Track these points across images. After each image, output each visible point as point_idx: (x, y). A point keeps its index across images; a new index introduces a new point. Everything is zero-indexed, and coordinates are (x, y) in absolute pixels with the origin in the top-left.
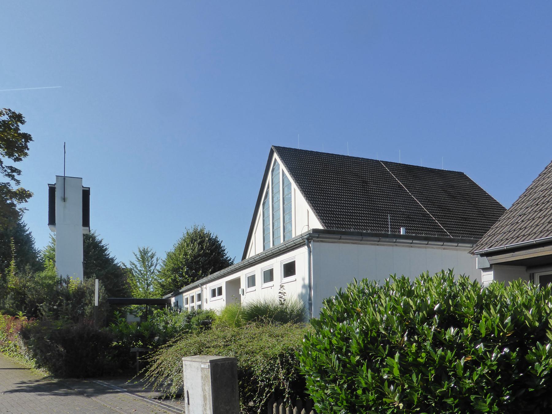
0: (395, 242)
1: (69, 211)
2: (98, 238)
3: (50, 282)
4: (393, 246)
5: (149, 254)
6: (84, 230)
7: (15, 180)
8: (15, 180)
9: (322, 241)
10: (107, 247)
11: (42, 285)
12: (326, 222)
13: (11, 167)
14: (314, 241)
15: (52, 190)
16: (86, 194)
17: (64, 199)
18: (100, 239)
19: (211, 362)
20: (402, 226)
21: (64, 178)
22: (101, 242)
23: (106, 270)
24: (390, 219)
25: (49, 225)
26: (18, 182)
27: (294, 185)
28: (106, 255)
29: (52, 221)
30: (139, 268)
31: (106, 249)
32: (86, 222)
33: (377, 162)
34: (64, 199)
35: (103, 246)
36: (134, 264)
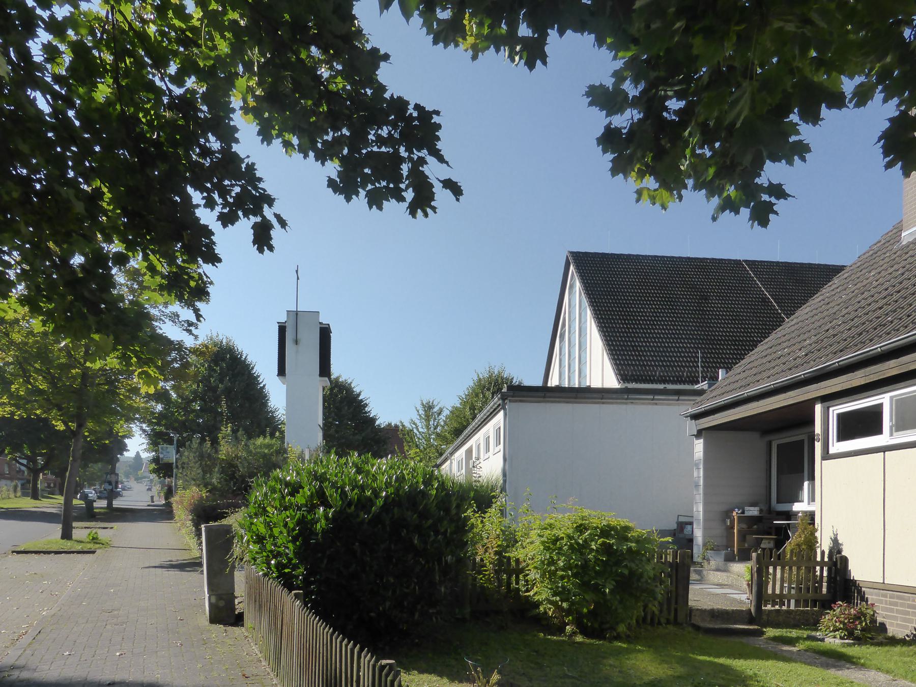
0: (627, 399)
1: (305, 356)
2: (357, 390)
3: (266, 451)
4: (626, 403)
5: (435, 410)
6: (326, 382)
7: (193, 335)
8: (193, 335)
9: (521, 401)
10: (367, 402)
11: (255, 454)
12: (620, 364)
13: (188, 321)
14: (510, 401)
15: (282, 329)
16: (325, 334)
17: (296, 342)
18: (358, 391)
19: (817, 630)
20: (721, 368)
21: (297, 313)
22: (359, 395)
23: (363, 434)
24: (702, 361)
25: (278, 375)
26: (196, 337)
27: (589, 313)
28: (366, 413)
29: (282, 371)
30: (421, 430)
31: (366, 405)
32: (325, 368)
33: (738, 263)
34: (296, 342)
35: (362, 401)
36: (414, 424)
